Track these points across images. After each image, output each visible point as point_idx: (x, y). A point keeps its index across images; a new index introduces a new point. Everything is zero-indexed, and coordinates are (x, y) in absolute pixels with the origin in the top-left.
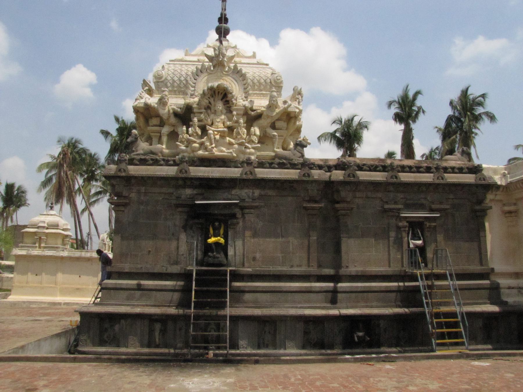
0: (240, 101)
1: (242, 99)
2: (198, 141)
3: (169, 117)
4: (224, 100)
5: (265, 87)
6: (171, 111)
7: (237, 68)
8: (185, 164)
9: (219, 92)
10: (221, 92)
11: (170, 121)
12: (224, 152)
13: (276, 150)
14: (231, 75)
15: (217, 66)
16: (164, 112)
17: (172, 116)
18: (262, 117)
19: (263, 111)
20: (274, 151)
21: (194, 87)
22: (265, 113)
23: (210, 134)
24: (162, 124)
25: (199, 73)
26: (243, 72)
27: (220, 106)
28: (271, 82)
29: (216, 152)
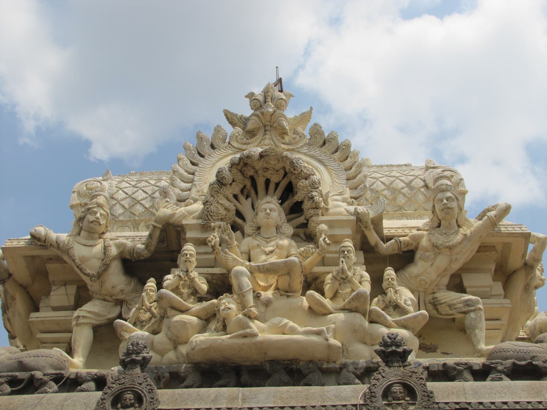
0: (335, 199)
1: (344, 200)
2: (197, 307)
3: (106, 267)
4: (288, 203)
5: (410, 200)
6: (114, 251)
7: (322, 134)
8: (138, 370)
9: (267, 182)
10: (275, 179)
11: (108, 285)
12: (293, 331)
13: (483, 346)
14: (305, 150)
15: (261, 132)
16: (88, 254)
17: (116, 267)
18: (418, 255)
19: (417, 239)
20: (480, 354)
21: (192, 181)
22: (424, 242)
23: (241, 273)
24: (82, 297)
25: (207, 150)
26: (340, 140)
27: (270, 208)
28: (426, 186)
29: (264, 332)
